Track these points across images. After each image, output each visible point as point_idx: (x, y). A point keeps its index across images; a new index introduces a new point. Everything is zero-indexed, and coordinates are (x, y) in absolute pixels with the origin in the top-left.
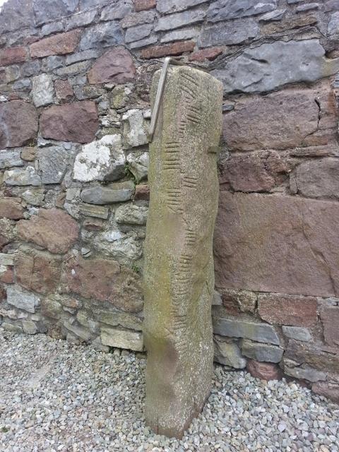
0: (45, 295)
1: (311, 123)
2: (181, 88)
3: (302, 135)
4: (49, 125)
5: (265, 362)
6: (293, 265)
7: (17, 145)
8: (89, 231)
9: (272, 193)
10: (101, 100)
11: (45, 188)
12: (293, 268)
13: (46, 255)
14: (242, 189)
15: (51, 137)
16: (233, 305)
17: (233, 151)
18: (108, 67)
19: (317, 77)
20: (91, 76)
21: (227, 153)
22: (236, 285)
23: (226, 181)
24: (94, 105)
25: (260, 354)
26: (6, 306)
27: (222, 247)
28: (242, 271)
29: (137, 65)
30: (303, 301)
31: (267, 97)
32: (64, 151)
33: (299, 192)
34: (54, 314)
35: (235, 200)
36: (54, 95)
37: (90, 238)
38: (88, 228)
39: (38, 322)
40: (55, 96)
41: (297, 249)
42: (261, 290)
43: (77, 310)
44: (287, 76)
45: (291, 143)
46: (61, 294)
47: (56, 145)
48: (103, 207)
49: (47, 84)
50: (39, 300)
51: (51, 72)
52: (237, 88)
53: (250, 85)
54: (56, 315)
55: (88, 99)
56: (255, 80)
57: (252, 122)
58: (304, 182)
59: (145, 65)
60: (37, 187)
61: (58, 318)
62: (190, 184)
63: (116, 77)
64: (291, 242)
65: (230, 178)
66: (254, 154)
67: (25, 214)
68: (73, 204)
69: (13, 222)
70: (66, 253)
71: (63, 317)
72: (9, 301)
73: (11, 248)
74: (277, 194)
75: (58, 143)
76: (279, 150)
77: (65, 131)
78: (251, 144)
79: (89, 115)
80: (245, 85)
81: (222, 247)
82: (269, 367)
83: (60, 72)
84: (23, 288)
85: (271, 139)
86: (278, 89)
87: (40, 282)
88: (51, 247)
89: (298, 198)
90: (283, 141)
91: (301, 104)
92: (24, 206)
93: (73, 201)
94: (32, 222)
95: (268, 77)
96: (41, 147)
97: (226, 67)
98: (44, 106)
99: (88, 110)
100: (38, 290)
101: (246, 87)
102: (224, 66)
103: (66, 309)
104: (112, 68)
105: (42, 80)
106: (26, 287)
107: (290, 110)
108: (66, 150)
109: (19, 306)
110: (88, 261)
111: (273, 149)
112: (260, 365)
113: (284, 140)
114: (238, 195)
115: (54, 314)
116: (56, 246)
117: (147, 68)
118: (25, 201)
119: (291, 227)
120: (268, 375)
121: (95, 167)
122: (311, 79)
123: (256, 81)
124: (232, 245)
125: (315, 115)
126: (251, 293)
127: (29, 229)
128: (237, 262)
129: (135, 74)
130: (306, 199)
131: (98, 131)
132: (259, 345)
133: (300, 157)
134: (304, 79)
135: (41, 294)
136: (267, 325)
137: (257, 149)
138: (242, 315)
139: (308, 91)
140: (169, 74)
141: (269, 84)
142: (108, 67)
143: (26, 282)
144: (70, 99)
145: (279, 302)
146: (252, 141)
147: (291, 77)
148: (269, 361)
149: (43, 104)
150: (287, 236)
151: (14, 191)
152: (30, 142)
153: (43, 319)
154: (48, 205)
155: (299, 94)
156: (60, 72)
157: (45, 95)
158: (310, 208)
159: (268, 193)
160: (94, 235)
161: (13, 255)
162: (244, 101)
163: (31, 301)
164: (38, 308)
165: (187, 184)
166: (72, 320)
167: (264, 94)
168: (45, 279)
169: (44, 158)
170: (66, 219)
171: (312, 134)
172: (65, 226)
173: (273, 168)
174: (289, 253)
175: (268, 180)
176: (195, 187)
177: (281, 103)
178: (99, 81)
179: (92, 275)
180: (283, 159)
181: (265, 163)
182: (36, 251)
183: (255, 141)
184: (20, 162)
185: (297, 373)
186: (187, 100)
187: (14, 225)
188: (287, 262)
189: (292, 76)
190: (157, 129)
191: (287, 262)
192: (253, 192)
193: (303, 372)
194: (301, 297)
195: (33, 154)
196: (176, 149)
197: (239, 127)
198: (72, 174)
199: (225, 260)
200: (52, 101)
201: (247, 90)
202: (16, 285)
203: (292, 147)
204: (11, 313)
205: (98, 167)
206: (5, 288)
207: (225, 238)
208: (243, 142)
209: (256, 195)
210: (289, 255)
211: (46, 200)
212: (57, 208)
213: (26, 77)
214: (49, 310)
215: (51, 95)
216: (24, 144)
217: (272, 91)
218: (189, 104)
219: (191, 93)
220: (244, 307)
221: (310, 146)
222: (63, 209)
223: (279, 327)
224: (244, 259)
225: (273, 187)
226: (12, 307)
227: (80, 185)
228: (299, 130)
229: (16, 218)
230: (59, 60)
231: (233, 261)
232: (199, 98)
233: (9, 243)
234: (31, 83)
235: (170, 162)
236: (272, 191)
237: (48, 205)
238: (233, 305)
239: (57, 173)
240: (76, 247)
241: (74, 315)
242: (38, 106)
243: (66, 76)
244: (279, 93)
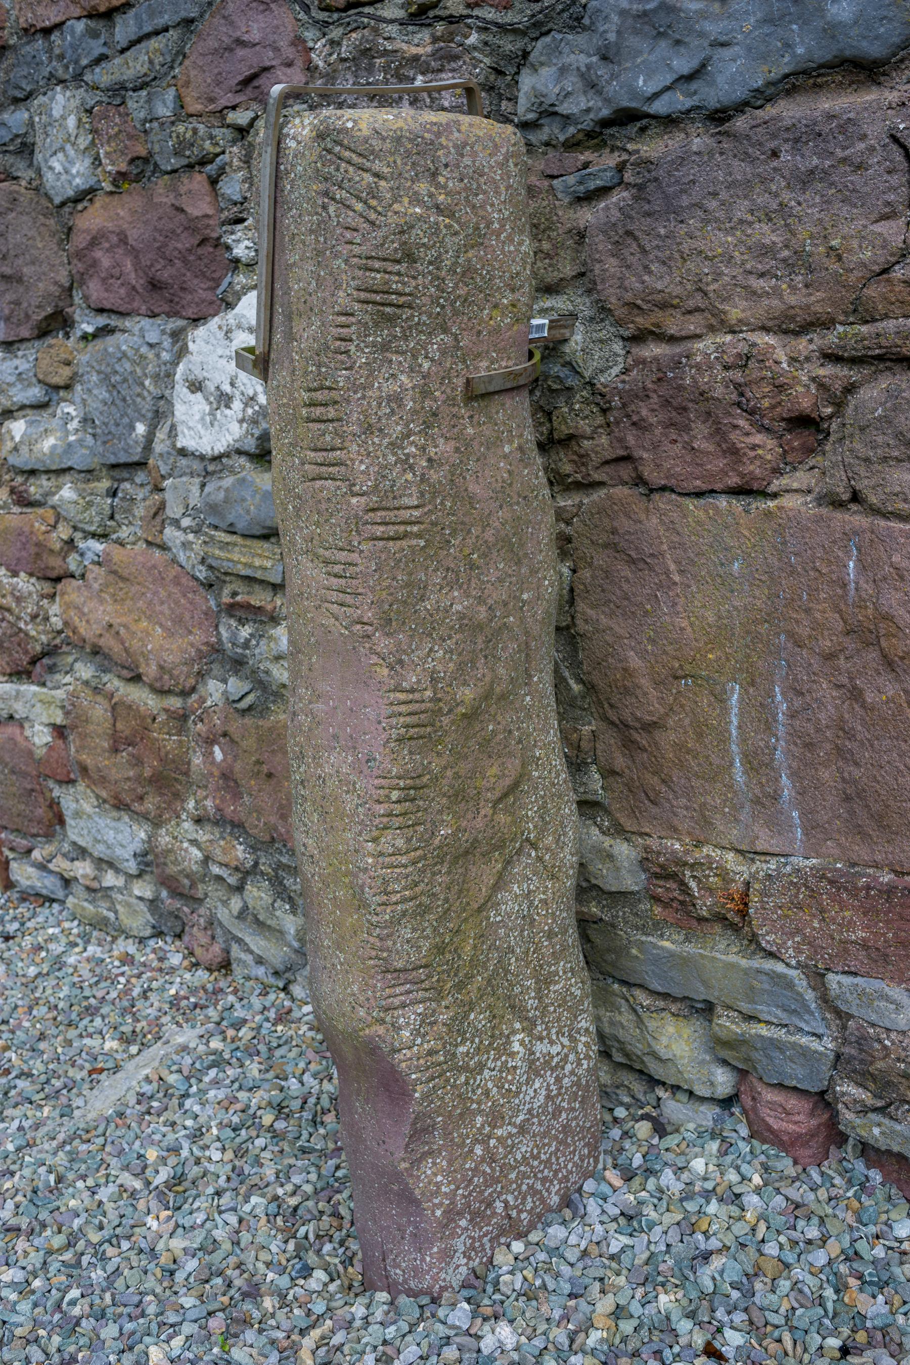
0: (157, 823)
1: (878, 228)
2: (326, 194)
3: (852, 278)
4: (95, 263)
5: (781, 1086)
6: (856, 764)
7: (25, 333)
8: (242, 622)
9: (775, 496)
10: (222, 171)
11: (114, 479)
12: (857, 773)
13: (141, 697)
14: (673, 482)
15: (108, 306)
16: (676, 894)
17: (639, 338)
18: (229, 49)
19: (896, 40)
20: (187, 84)
21: (618, 347)
22: (684, 826)
23: (621, 453)
24: (207, 187)
25: (765, 1061)
26: (66, 847)
27: (627, 691)
28: (696, 775)
29: (309, 35)
30: (889, 891)
31: (726, 134)
32: (144, 350)
33: (856, 497)
34: (186, 882)
35: (655, 520)
36: (97, 162)
37: (246, 645)
38: (240, 611)
39: (152, 901)
40: (100, 164)
41: (863, 706)
42: (759, 849)
43: (246, 874)
44: (788, 46)
45: (818, 308)
46: (198, 821)
47: (124, 331)
48: (266, 545)
49: (71, 122)
50: (143, 835)
51: (78, 77)
52: (625, 103)
53: (668, 89)
54: (193, 885)
55: (190, 166)
56: (683, 64)
57: (682, 230)
58: (867, 460)
59: (335, 33)
60: (89, 473)
61: (200, 895)
62: (391, 530)
63: (256, 83)
64: (845, 681)
65: (631, 440)
66: (705, 346)
67: (72, 563)
68: (185, 530)
69: (47, 587)
70: (193, 689)
71: (214, 892)
72: (73, 835)
73: (51, 669)
74: (790, 502)
75: (128, 323)
76: (786, 332)
77: (139, 283)
78: (690, 312)
79: (192, 225)
80: (651, 89)
81: (627, 691)
82: (792, 1102)
83: (103, 76)
84: (98, 797)
85: (753, 294)
86: (762, 97)
87: (139, 779)
88: (150, 671)
89: (856, 519)
90: (792, 300)
91: (840, 153)
92: (65, 537)
93: (186, 522)
94: (88, 587)
95: (727, 53)
96: (85, 337)
97: (586, 21)
98: (76, 200)
99: (189, 210)
100: (136, 806)
101: (656, 95)
102: (579, 19)
103: (216, 870)
104: (241, 52)
105: (57, 112)
106: (104, 794)
107: (805, 180)
108: (151, 346)
109: (99, 850)
110: (248, 721)
111: (765, 329)
112: (769, 1095)
113: (794, 296)
114: (662, 501)
115: (186, 882)
116: (161, 667)
117: (339, 44)
118: (65, 519)
119: (840, 626)
120: (791, 1127)
121: (228, 407)
122: (874, 50)
123: (686, 71)
124: (657, 684)
125: (892, 197)
126: (730, 856)
127: (87, 609)
128: (680, 747)
129: (310, 69)
130: (883, 523)
131: (228, 279)
132: (763, 1030)
133: (854, 361)
134: (848, 53)
135: (145, 817)
136: (780, 968)
137: (712, 329)
138: (707, 927)
139: (871, 96)
140: (292, 144)
141: (724, 87)
142: (229, 49)
143: (103, 780)
144: (139, 171)
145: (813, 894)
146: (691, 304)
147: (800, 51)
148: (794, 1083)
149: (71, 193)
150: (830, 657)
151: (34, 489)
152: (56, 322)
153: (164, 894)
154: (124, 533)
155: (831, 117)
156: (103, 76)
157: (72, 163)
158: (896, 559)
159: (764, 494)
160: (259, 636)
161: (60, 694)
162: (654, 147)
163: (125, 837)
164: (149, 861)
165: (379, 530)
166: (236, 904)
167: (719, 117)
168: (147, 772)
169: (95, 378)
170: (176, 581)
171: (885, 271)
172: (177, 603)
173: (766, 403)
174: (841, 718)
175: (754, 447)
176: (419, 536)
177: (775, 154)
178: (212, 100)
179: (265, 769)
180: (796, 367)
181: (737, 386)
182: (116, 682)
183: (698, 301)
184: (35, 393)
185: (876, 1131)
186: (348, 235)
187: (52, 597)
188: (839, 751)
189: (804, 47)
190: (278, 337)
191: (839, 751)
192: (713, 491)
193: (893, 1132)
194: (886, 878)
195: (68, 363)
196: (331, 413)
197: (644, 251)
198: (173, 432)
199: (642, 739)
200: (92, 181)
201: (659, 107)
202: (81, 787)
203: (827, 324)
204: (83, 869)
205: (237, 405)
206: (56, 793)
207: (635, 661)
208: (664, 306)
209: (723, 502)
210: (840, 725)
211: (117, 517)
212: (149, 543)
213: (16, 101)
214: (172, 869)
215: (88, 161)
216: (43, 332)
217: (741, 107)
218: (357, 250)
219: (359, 207)
220: (705, 905)
221: (886, 316)
222: (163, 547)
223: (817, 978)
224: (700, 735)
225: (777, 472)
226: (82, 853)
227: (197, 466)
228: (839, 258)
229: (54, 574)
230: (95, 35)
231: (667, 739)
232: (392, 219)
233: (44, 654)
234: (31, 124)
235: (320, 457)
236: (773, 488)
237: (124, 533)
238: (676, 894)
239: (133, 428)
240: (215, 672)
241: (239, 889)
242: (57, 200)
243: (119, 90)
244: (770, 111)
